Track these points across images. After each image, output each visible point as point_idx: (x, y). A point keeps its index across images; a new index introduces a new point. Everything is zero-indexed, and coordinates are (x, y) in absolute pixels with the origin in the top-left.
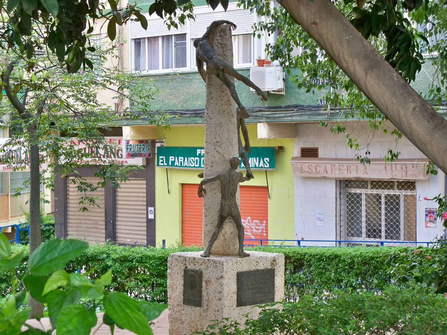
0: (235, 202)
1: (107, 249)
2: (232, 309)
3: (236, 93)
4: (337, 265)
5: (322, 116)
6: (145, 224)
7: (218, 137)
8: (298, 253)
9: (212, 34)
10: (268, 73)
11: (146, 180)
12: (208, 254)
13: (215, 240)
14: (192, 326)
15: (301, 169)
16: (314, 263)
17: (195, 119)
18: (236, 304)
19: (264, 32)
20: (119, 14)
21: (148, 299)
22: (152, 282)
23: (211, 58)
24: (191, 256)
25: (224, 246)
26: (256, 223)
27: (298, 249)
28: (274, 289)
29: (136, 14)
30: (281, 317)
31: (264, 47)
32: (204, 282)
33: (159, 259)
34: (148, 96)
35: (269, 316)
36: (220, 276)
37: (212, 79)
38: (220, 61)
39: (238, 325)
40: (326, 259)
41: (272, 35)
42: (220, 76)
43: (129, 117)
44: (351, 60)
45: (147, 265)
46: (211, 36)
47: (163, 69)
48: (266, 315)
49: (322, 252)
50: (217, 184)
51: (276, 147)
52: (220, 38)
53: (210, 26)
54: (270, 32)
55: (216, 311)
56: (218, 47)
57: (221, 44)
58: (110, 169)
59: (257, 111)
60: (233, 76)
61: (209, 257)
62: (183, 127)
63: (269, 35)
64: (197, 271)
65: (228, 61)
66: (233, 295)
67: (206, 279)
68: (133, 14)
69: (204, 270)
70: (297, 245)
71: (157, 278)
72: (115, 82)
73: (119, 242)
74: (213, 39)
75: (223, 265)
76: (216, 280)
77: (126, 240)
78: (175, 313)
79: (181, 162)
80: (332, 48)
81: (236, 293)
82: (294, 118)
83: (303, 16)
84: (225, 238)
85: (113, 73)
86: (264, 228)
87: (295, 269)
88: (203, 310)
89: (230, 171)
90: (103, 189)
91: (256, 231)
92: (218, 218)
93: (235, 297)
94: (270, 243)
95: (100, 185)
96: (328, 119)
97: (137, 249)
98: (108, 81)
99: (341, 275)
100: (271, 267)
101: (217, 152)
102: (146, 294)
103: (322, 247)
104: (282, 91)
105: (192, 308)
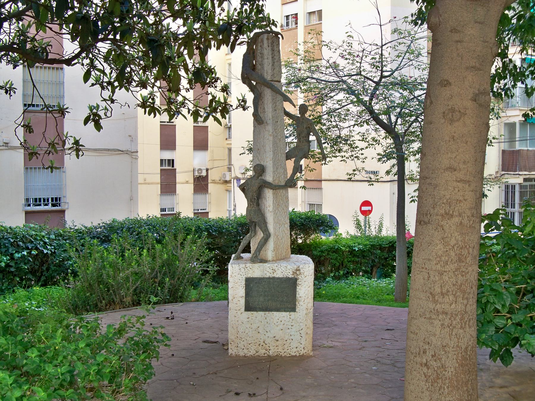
2: (239, 312)
66: (240, 299)
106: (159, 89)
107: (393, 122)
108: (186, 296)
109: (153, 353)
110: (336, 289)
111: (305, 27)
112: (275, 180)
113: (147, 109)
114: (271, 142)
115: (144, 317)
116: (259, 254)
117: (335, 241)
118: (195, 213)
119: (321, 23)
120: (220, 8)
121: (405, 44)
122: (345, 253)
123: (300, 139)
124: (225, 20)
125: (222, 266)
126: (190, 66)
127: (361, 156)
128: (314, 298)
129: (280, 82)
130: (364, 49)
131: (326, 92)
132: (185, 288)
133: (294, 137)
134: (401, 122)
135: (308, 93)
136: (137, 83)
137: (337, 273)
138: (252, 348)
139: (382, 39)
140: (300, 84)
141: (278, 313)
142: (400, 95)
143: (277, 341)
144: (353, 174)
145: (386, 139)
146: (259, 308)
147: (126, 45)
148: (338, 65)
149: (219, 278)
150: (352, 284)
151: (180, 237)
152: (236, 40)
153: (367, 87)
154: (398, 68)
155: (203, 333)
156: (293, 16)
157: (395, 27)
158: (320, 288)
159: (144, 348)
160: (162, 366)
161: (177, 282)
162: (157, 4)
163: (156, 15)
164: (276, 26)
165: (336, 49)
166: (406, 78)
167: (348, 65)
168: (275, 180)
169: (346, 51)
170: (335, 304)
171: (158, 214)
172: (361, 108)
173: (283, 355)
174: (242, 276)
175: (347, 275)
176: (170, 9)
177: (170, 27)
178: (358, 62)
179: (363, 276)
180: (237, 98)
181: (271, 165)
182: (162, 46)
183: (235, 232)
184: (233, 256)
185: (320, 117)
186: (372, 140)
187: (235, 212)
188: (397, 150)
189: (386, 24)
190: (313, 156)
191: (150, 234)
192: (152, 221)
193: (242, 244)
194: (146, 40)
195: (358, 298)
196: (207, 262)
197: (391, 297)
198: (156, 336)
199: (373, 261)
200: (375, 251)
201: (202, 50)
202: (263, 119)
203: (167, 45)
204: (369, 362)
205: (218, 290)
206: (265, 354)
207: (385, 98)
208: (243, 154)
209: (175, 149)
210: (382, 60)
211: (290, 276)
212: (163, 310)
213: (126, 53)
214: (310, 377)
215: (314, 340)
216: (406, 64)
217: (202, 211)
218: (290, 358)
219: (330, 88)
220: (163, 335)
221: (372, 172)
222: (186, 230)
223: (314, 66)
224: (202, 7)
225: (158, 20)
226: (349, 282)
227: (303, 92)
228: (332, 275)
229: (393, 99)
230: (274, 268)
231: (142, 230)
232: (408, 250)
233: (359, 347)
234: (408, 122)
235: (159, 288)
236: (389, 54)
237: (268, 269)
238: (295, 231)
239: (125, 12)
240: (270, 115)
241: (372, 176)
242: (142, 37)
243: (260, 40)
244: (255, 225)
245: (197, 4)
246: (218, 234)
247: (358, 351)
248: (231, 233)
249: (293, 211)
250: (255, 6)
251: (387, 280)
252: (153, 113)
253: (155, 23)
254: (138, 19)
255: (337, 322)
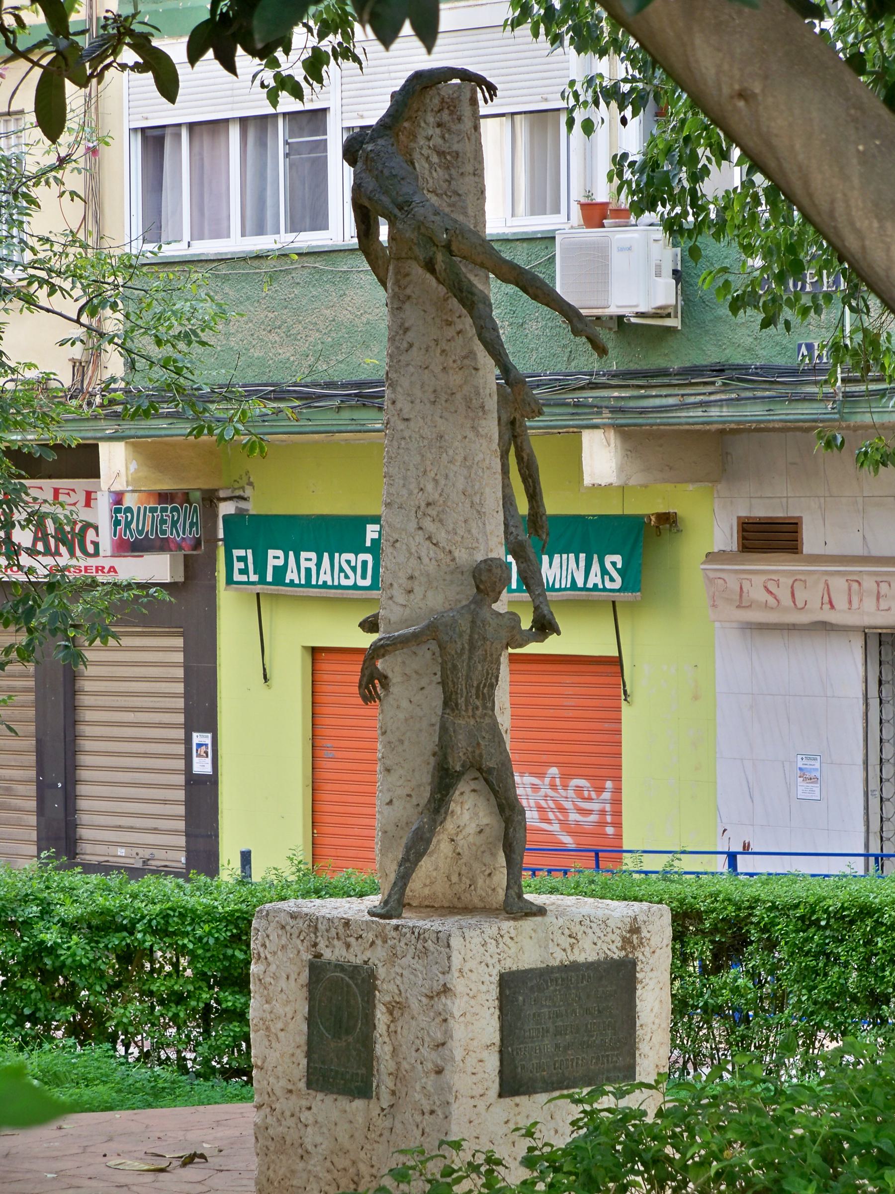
0: (493, 718)
1: (42, 886)
2: (482, 1106)
3: (495, 329)
4: (868, 943)
5: (815, 405)
6: (181, 795)
7: (430, 487)
8: (729, 900)
9: (409, 119)
10: (621, 250)
11: (182, 634)
12: (388, 911)
13: (420, 856)
14: (340, 1167)
15: (741, 596)
16: (787, 933)
17: (357, 415)
18: (495, 1087)
19: (606, 112)
20: (74, 45)
21: (189, 1064)
22: (202, 1005)
23: (404, 206)
24: (335, 913)
25: (455, 878)
26: (579, 790)
27: (726, 886)
28: (635, 1031)
29: (134, 47)
30: (653, 1139)
31: (604, 165)
32: (384, 1009)
33: (229, 922)
34: (187, 335)
35: (607, 1133)
36: (437, 987)
37: (408, 279)
38: (436, 213)
39: (500, 1169)
40: (828, 919)
41: (634, 124)
42: (437, 267)
43: (119, 408)
44: (876, 224)
45: (186, 941)
46: (406, 124)
47: (243, 235)
48: (596, 1128)
49: (813, 894)
50: (428, 655)
51: (649, 516)
52: (438, 131)
53: (401, 90)
54: (628, 112)
55: (423, 1114)
56: (431, 164)
57: (441, 154)
58: (47, 599)
59: (582, 388)
60: (482, 265)
61: (399, 916)
62: (316, 442)
63: (624, 121)
64: (356, 967)
65: (465, 214)
66: (485, 1055)
67: (388, 998)
68: (128, 45)
69: (380, 965)
70: (725, 869)
71: (221, 989)
72: (67, 285)
73: (87, 857)
74: (413, 136)
75: (449, 946)
76: (424, 999)
77: (112, 850)
78: (278, 1120)
79: (308, 570)
80: (806, 184)
81: (497, 1049)
82: (714, 412)
83: (704, 70)
84: (459, 850)
85: (61, 254)
86: (608, 807)
87: (716, 956)
88: (378, 1111)
89: (473, 606)
90: (31, 668)
91: (578, 817)
92: (433, 776)
93: (493, 1062)
94: (629, 862)
95: (14, 655)
96: (837, 416)
97: (149, 885)
98: (42, 282)
99: (884, 977)
100: (623, 953)
101: (429, 538)
102: (180, 1048)
103: (813, 876)
104: (668, 316)
105: (338, 1103)
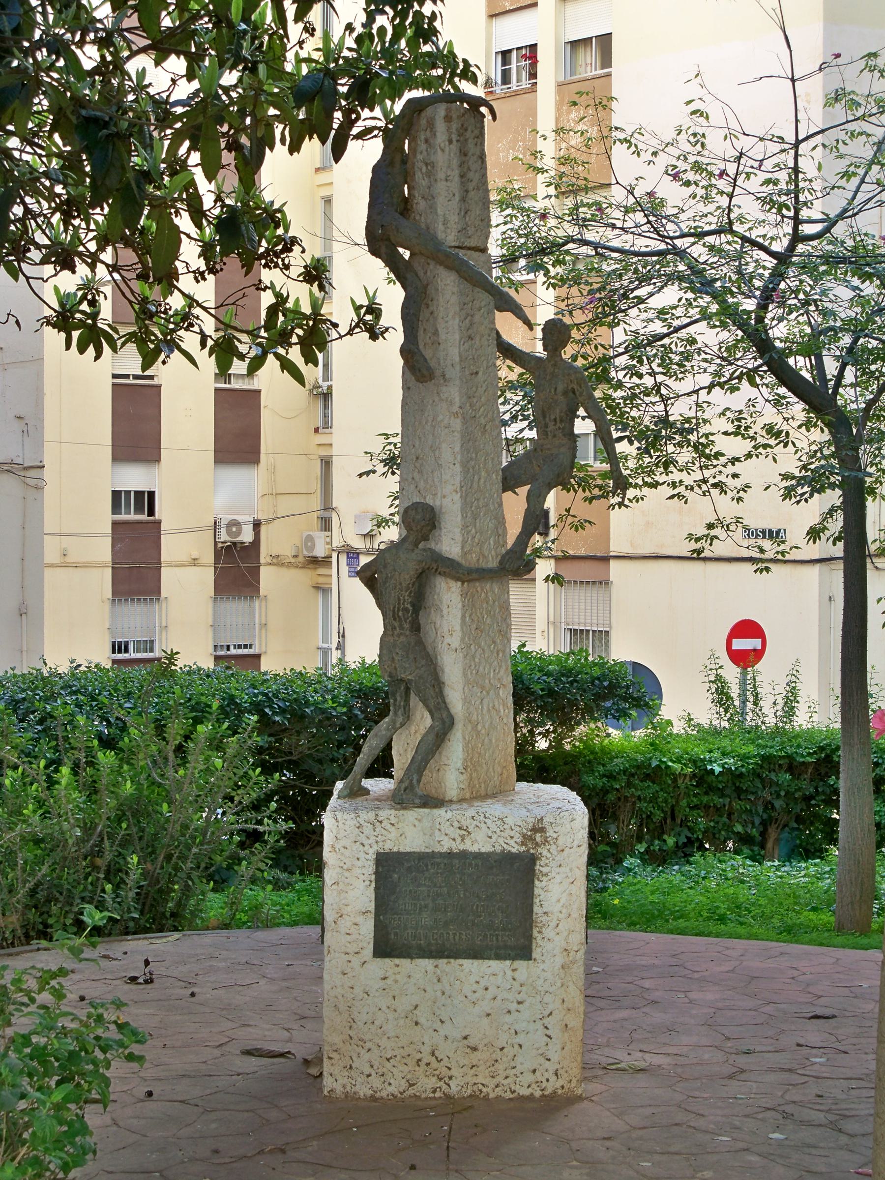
2: (356, 961)
66: (360, 919)
106: (110, 273)
107: (829, 377)
108: (192, 912)
109: (90, 1083)
110: (653, 893)
111: (560, 85)
112: (470, 552)
113: (76, 334)
114: (457, 435)
115: (62, 972)
116: (419, 781)
117: (652, 744)
118: (217, 658)
119: (609, 75)
120: (301, 25)
121: (868, 135)
122: (680, 781)
123: (546, 426)
124: (317, 62)
125: (302, 821)
126: (208, 201)
127: (730, 482)
128: (587, 918)
129: (484, 250)
130: (741, 154)
131: (625, 283)
132: (187, 885)
133: (526, 423)
134: (856, 377)
135: (570, 286)
136: (44, 251)
137: (657, 842)
138: (395, 1070)
139: (797, 121)
140: (546, 260)
141: (476, 962)
142: (852, 294)
143: (474, 1049)
144: (707, 536)
145: (808, 431)
146: (420, 947)
147: (10, 134)
148: (662, 203)
149: (293, 856)
150: (704, 878)
151: (175, 729)
152: (348, 123)
153: (750, 268)
154: (845, 210)
155: (244, 1025)
156: (524, 52)
157: (838, 85)
158: (605, 889)
159: (62, 1067)
160: (115, 1128)
161: (162, 868)
162: (107, 9)
163: (103, 43)
164: (474, 80)
165: (655, 154)
166: (871, 241)
167: (692, 202)
168: (470, 552)
169: (686, 159)
170: (653, 937)
171: (103, 657)
172: (731, 335)
173: (492, 1096)
174: (367, 847)
175: (688, 850)
176: (149, 23)
177: (146, 82)
178: (722, 193)
179: (737, 852)
180: (352, 300)
181: (457, 507)
182: (124, 137)
183: (344, 714)
184: (339, 785)
185: (606, 360)
186: (764, 433)
187: (343, 653)
188: (841, 461)
189: (810, 75)
190: (584, 483)
191: (81, 720)
192: (86, 679)
193: (365, 749)
194: (73, 119)
195: (722, 919)
196: (256, 806)
197: (827, 917)
198: (100, 1032)
199: (768, 806)
200: (773, 776)
201: (246, 152)
202: (432, 364)
203: (136, 135)
204: (760, 1116)
205: (287, 896)
206: (434, 1092)
207: (806, 303)
208: (368, 473)
209: (158, 460)
210: (797, 186)
211: (515, 849)
212: (119, 955)
213: (11, 158)
214: (575, 1163)
215: (587, 1048)
216: (870, 199)
217: (240, 652)
218: (512, 1105)
219: (636, 271)
220: (121, 1027)
221: (764, 532)
222: (193, 709)
223: (589, 206)
224: (246, 19)
225: (109, 58)
226: (694, 871)
227: (554, 286)
228: (641, 848)
229: (829, 305)
230: (464, 824)
231: (59, 708)
232: (878, 771)
233: (727, 1070)
234: (877, 379)
235: (109, 887)
236: (819, 168)
237: (445, 828)
238: (528, 712)
239: (8, 34)
240: (454, 353)
241: (766, 544)
242: (61, 109)
243: (423, 122)
244: (407, 690)
245: (229, 10)
246: (288, 720)
247: (726, 1082)
248: (330, 718)
249: (520, 652)
250: (410, 19)
251: (812, 866)
252: (91, 346)
253: (102, 68)
254: (49, 55)
255: (657, 994)
